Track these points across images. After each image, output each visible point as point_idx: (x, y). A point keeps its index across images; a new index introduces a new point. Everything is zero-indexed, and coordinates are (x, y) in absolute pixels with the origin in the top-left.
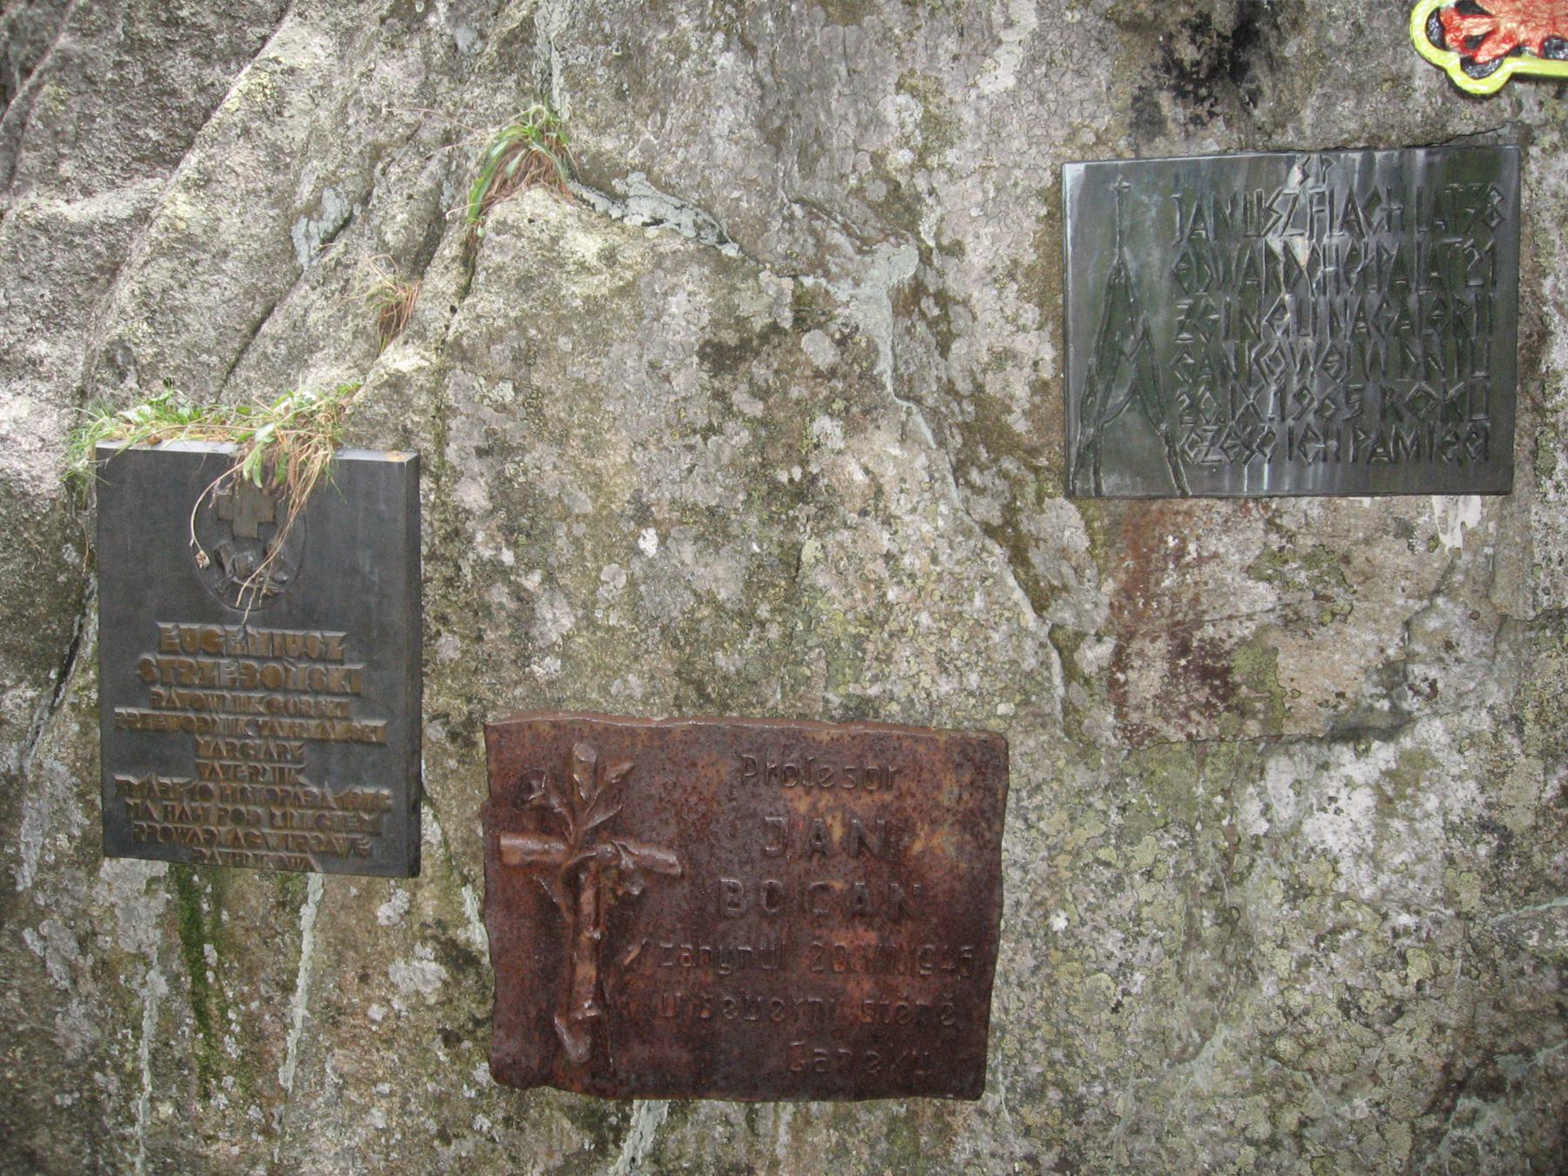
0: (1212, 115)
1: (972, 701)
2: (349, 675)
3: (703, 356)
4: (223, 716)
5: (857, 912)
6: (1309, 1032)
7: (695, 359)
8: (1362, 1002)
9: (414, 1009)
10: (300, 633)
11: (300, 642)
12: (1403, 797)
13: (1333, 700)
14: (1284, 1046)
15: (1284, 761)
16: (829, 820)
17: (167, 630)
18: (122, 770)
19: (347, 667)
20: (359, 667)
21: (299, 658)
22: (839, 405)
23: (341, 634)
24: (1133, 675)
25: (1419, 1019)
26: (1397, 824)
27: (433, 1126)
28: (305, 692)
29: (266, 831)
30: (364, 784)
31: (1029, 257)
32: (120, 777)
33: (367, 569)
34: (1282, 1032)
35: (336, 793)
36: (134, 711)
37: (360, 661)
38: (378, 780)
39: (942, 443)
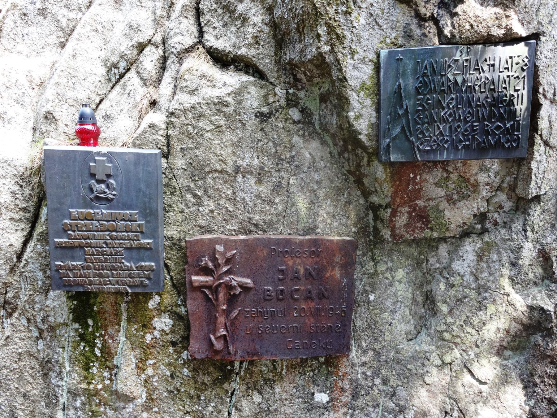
1: (344, 228)
2: (139, 226)
4: (94, 241)
5: (309, 298)
7: (254, 118)
9: (162, 335)
15: (444, 245)
16: (299, 267)
17: (74, 212)
18: (57, 261)
19: (138, 222)
20: (143, 222)
21: (121, 220)
24: (397, 218)
26: (484, 265)
27: (168, 374)
28: (124, 232)
29: (111, 279)
30: (145, 262)
31: (369, 83)
32: (57, 263)
33: (145, 189)
34: (445, 331)
35: (135, 264)
36: (62, 240)
38: (150, 261)
39: (335, 145)
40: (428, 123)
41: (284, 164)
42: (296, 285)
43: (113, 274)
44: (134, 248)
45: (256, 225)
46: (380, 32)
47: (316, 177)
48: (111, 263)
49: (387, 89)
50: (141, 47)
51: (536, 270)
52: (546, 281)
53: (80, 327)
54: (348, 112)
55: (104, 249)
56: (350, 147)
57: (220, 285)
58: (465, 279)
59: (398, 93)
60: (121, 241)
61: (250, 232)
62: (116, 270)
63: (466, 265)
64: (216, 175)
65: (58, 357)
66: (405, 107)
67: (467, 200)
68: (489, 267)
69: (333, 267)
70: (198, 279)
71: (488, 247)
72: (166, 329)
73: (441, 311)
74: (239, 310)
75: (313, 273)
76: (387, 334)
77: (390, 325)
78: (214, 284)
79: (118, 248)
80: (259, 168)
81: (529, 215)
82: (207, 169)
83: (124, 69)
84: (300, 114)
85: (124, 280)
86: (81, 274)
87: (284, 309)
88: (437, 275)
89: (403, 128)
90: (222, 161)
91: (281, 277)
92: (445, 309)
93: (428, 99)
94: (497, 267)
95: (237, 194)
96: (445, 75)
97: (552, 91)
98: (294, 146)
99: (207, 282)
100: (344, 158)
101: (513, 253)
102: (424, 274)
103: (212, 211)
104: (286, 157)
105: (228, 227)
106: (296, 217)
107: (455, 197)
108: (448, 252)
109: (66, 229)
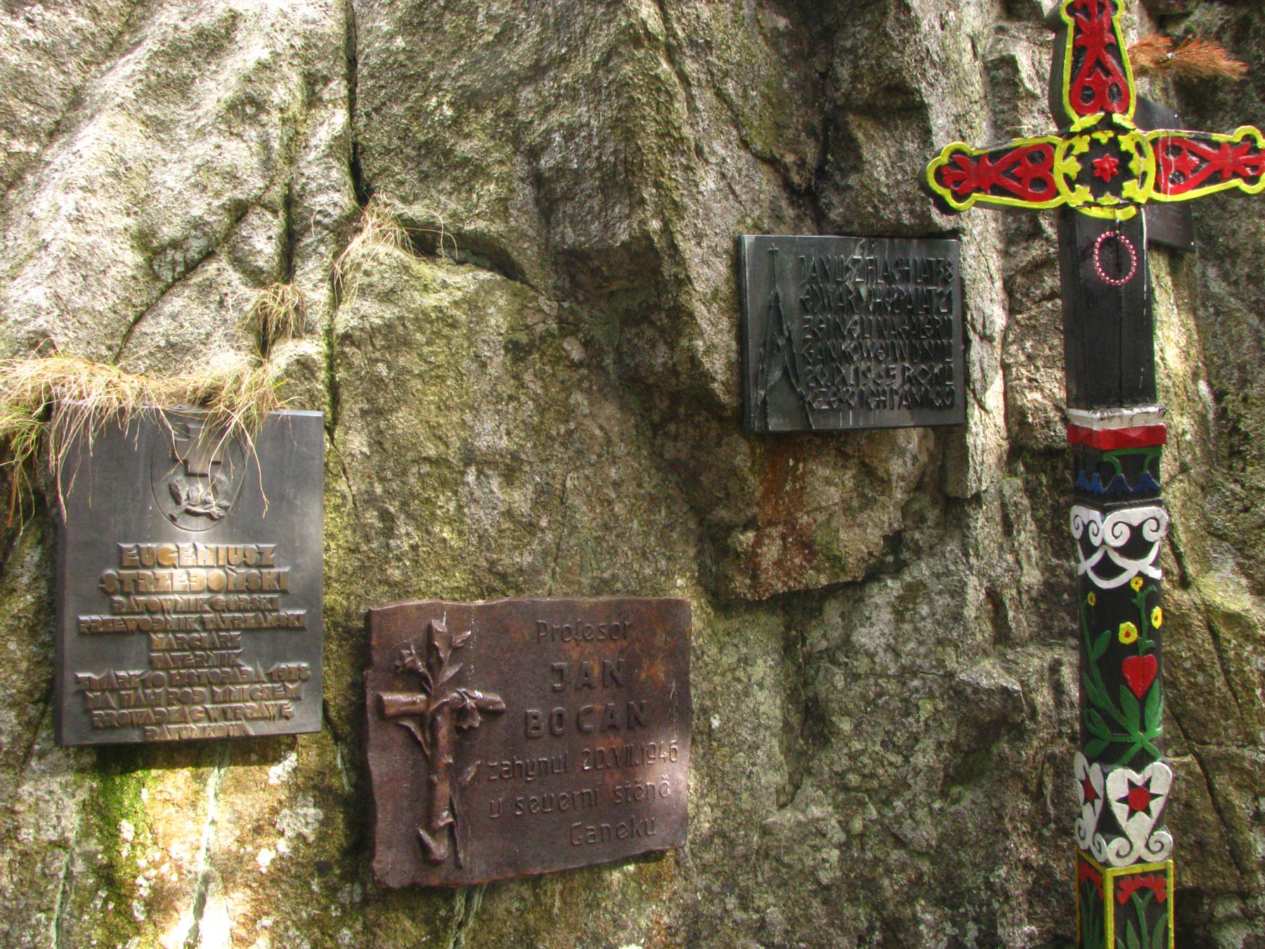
0: (805, 215)
3: (505, 348)
4: (174, 616)
6: (865, 766)
7: (502, 352)
8: (895, 739)
10: (240, 546)
11: (240, 553)
12: (907, 609)
13: (866, 557)
14: (853, 779)
15: (833, 601)
17: (130, 550)
18: (83, 669)
20: (287, 569)
22: (586, 384)
23: (273, 546)
24: (765, 549)
25: (928, 743)
26: (907, 627)
28: (243, 592)
29: (208, 706)
30: (288, 661)
31: (725, 290)
35: (265, 668)
37: (285, 565)
40: (822, 362)
41: (556, 446)
42: (586, 702)
43: (213, 693)
44: (267, 629)
45: (503, 577)
46: (737, 205)
47: (613, 473)
48: (210, 667)
49: (755, 304)
50: (239, 211)
51: (984, 628)
52: (1000, 647)
53: (101, 848)
54: (691, 340)
55: (196, 635)
56: (682, 410)
57: (439, 710)
58: (877, 660)
59: (775, 309)
60: (237, 615)
61: (492, 590)
62: (222, 684)
63: (877, 634)
64: (426, 468)
65: (34, 936)
66: (787, 334)
67: (872, 509)
68: (916, 629)
69: (653, 658)
70: (397, 698)
71: (914, 591)
72: (306, 831)
73: (838, 732)
74: (478, 766)
75: (618, 675)
76: (745, 796)
77: (749, 777)
78: (428, 706)
79: (227, 630)
80: (511, 454)
81: (969, 527)
82: (410, 455)
83: (200, 253)
84: (582, 349)
85: (240, 708)
86: (138, 698)
87: (565, 756)
88: (825, 664)
89: (785, 372)
90: (440, 438)
91: (558, 685)
92: (846, 726)
93: (821, 322)
94: (929, 626)
95: (466, 510)
96: (842, 282)
97: (981, 321)
98: (573, 411)
99: (414, 703)
100: (665, 434)
101: (953, 597)
102: (799, 667)
103: (414, 548)
104: (558, 434)
105: (446, 584)
106: (578, 558)
107: (855, 503)
108: (842, 616)
109: (111, 590)
